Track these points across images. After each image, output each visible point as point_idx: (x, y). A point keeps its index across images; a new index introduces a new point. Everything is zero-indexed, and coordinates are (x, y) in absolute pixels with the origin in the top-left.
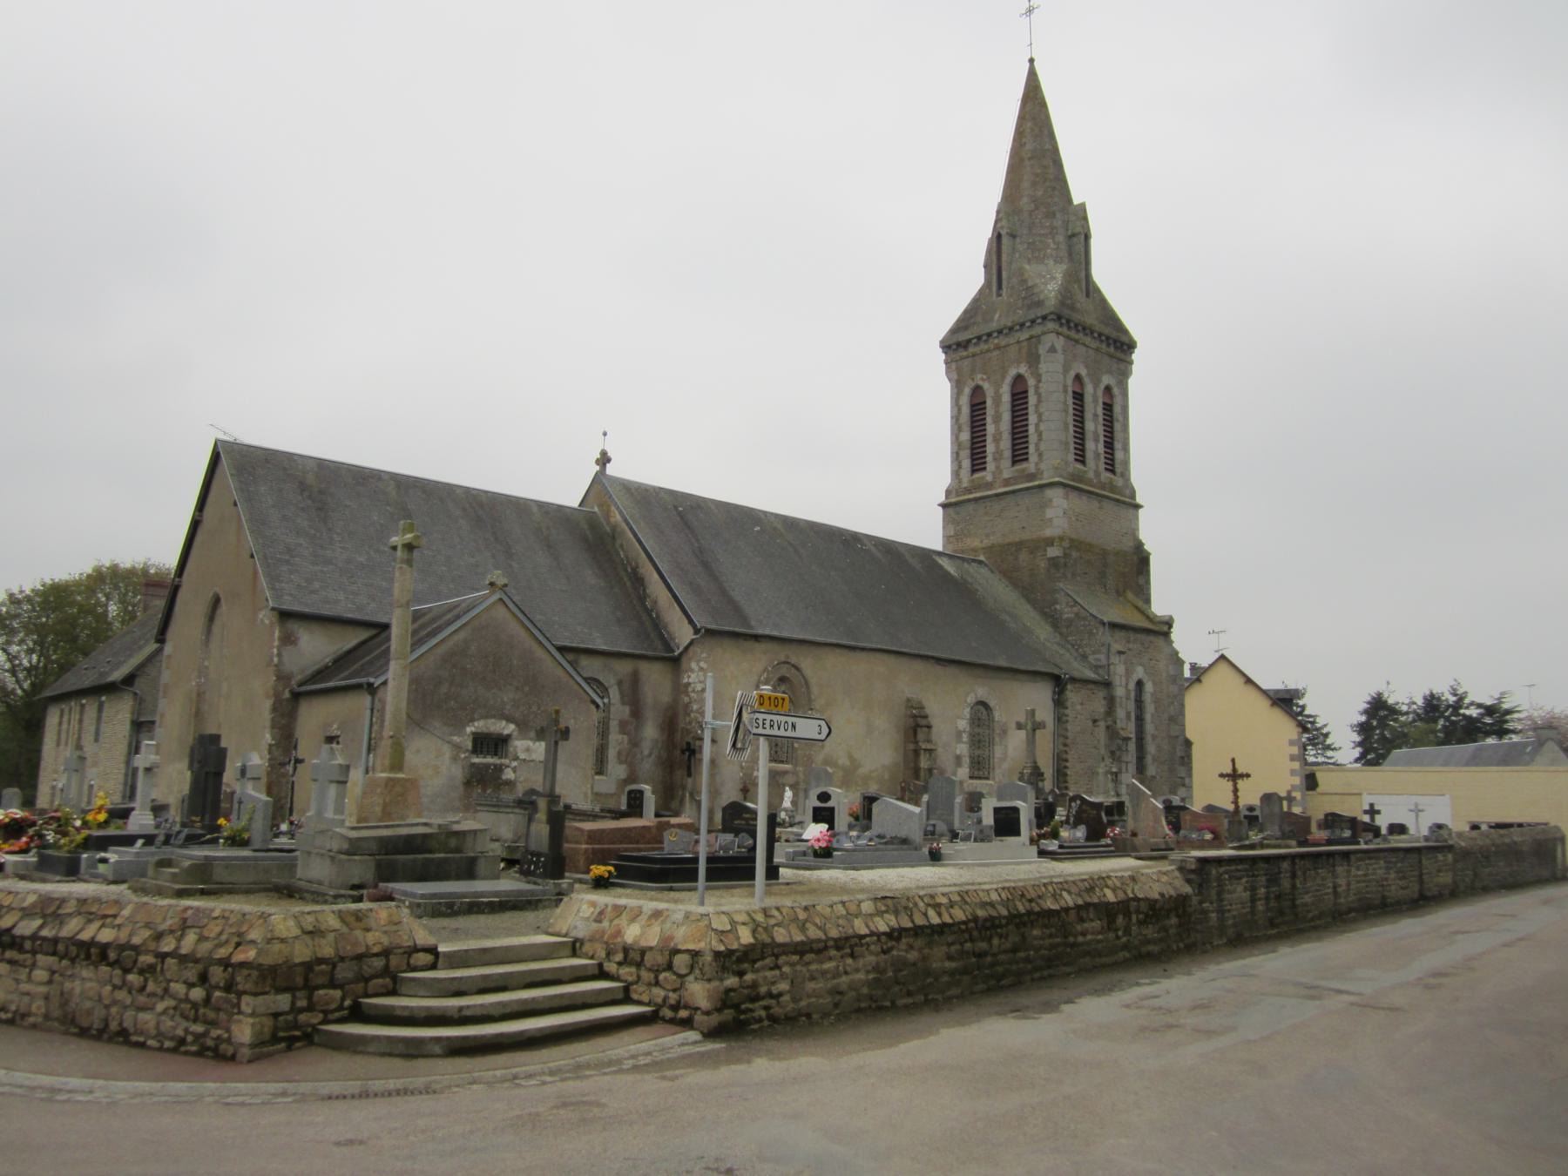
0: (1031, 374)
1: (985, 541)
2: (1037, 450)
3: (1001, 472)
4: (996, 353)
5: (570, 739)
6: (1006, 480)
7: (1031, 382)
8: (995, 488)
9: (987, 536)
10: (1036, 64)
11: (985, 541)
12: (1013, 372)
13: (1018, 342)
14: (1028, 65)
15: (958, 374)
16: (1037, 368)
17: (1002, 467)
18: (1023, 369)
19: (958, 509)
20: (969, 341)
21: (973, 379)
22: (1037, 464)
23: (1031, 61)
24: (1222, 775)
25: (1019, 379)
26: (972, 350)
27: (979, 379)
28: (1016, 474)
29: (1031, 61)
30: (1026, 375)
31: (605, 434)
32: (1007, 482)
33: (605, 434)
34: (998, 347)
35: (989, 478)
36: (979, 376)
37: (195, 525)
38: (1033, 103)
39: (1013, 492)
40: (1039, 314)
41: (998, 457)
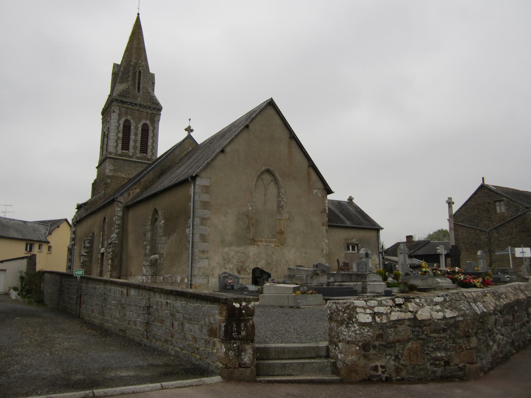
0: (151, 125)
1: (127, 176)
2: (152, 151)
3: (136, 154)
4: (137, 112)
5: (50, 242)
6: (137, 157)
7: (151, 128)
8: (132, 158)
9: (129, 174)
10: (140, 16)
11: (127, 176)
12: (144, 121)
13: (147, 112)
14: (137, 15)
15: (119, 111)
16: (154, 125)
17: (137, 152)
18: (148, 122)
19: (116, 160)
20: (127, 102)
21: (126, 117)
22: (151, 156)
23: (138, 14)
24: (520, 252)
25: (145, 125)
26: (126, 105)
27: (129, 117)
28: (142, 157)
29: (138, 14)
30: (149, 125)
31: (190, 120)
32: (138, 158)
33: (190, 120)
34: (138, 110)
35: (131, 154)
36: (129, 117)
37: (293, 137)
38: (137, 28)
39: (142, 163)
40: (157, 108)
41: (135, 148)
